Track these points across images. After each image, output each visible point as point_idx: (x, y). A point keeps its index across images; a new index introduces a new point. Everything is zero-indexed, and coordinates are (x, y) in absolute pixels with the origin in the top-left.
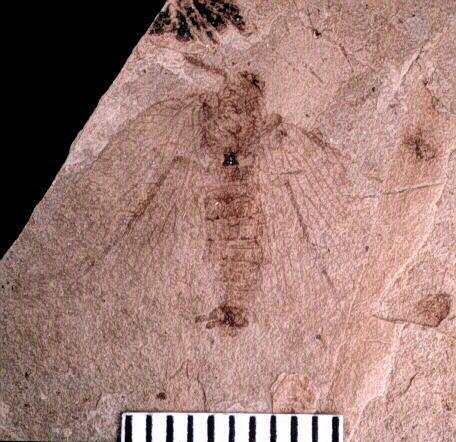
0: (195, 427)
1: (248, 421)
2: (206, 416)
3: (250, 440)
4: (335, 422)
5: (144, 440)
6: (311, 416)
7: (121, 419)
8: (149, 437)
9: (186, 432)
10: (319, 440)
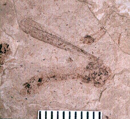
0: (59, 115)
1: (86, 113)
2: (62, 112)
3: (75, 118)
4: (100, 113)
5: (98, 118)
6: (81, 111)
7: (38, 112)
9: (57, 116)
10: (53, 118)
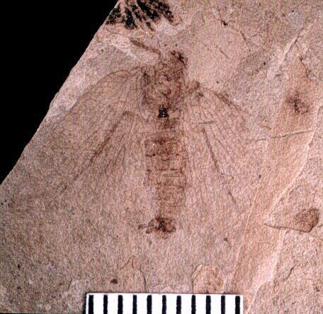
0: (138, 303)
1: (176, 299)
2: (146, 295)
3: (177, 313)
4: (238, 300)
5: (102, 312)
6: (220, 296)
7: (86, 297)
8: (105, 311)
9: (132, 307)
10: (226, 313)
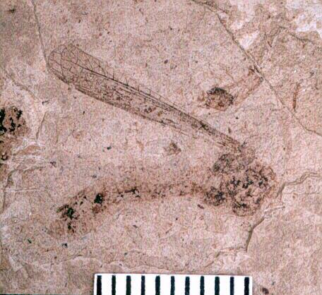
0: (146, 284)
1: (214, 280)
2: (154, 276)
3: (186, 294)
4: (247, 281)
5: (243, 293)
6: (200, 276)
7: (94, 278)
8: (114, 292)
9: (140, 288)
10: (235, 294)
